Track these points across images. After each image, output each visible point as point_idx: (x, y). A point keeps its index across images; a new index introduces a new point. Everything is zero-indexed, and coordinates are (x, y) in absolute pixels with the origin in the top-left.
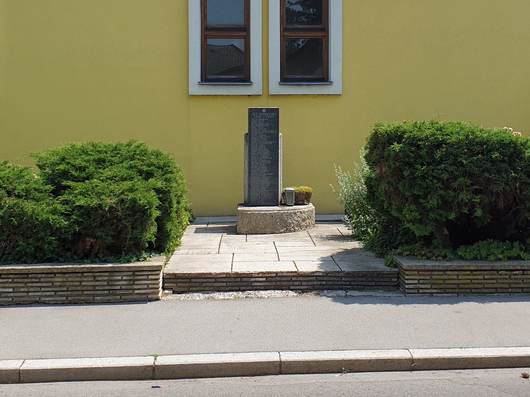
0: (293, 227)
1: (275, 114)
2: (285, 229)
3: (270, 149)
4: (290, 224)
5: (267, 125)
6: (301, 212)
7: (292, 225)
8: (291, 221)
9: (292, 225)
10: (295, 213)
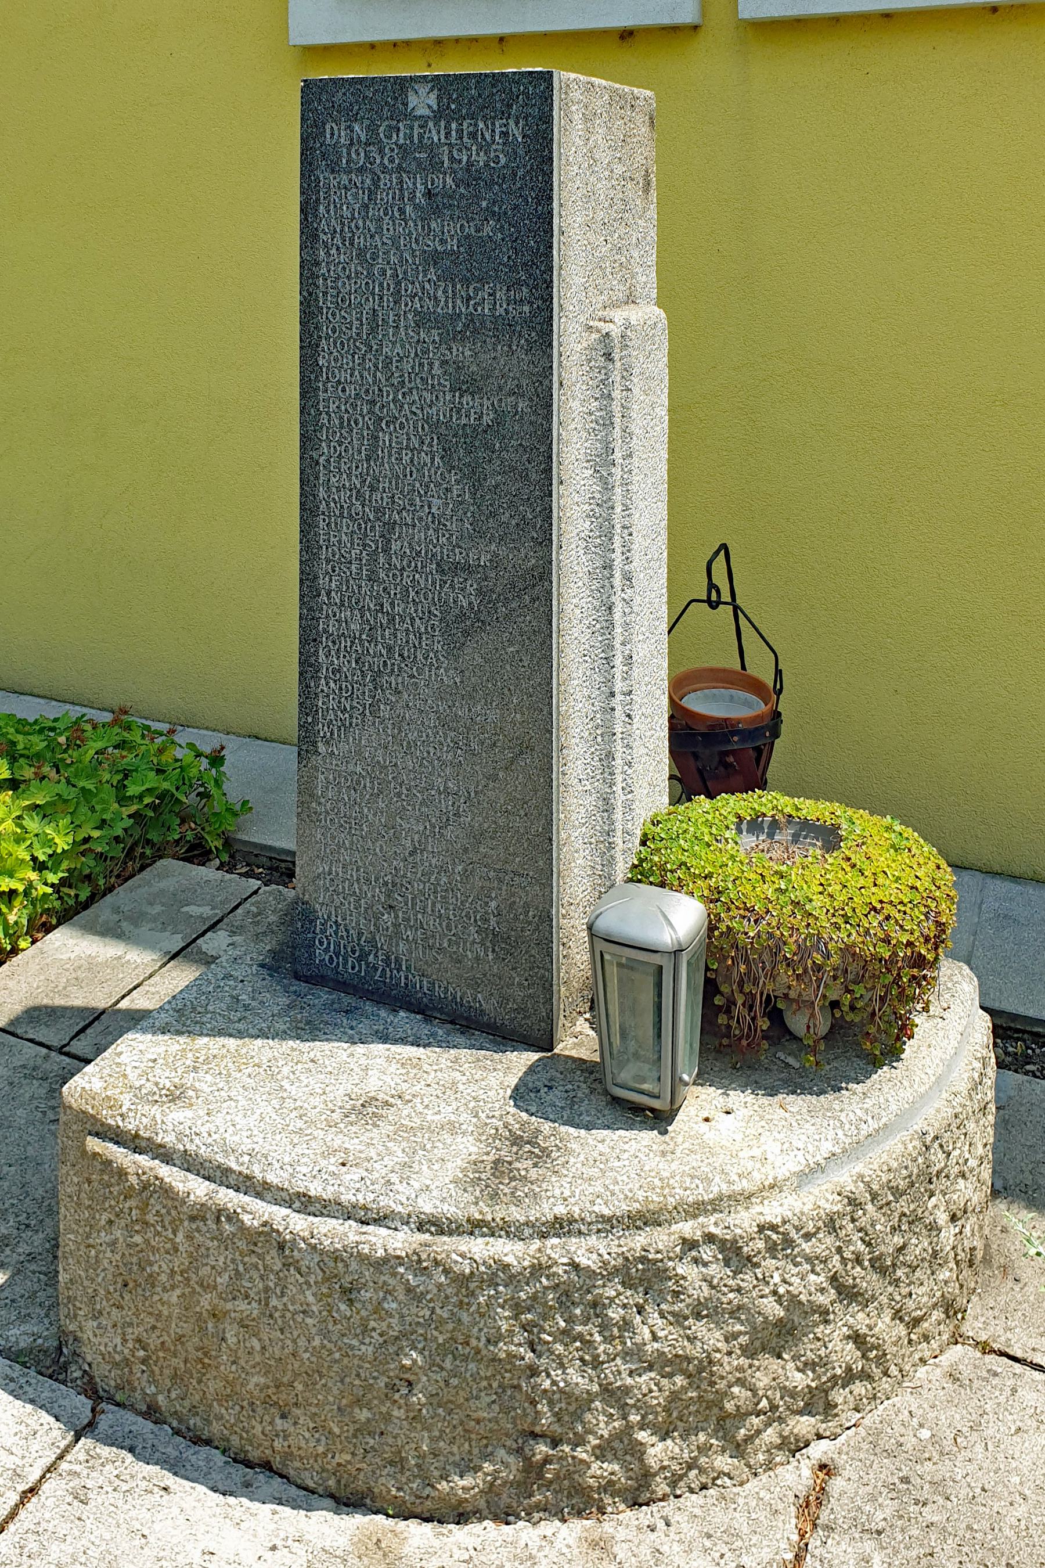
0: (622, 1447)
1: (516, 131)
2: (501, 1467)
3: (474, 477)
4: (573, 1407)
5: (449, 233)
6: (733, 1253)
7: (602, 1424)
8: (577, 1379)
9: (602, 1424)
10: (647, 1277)
